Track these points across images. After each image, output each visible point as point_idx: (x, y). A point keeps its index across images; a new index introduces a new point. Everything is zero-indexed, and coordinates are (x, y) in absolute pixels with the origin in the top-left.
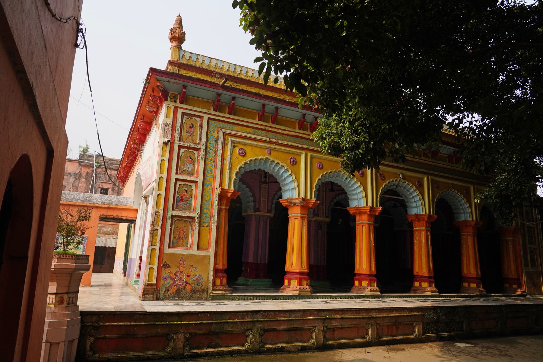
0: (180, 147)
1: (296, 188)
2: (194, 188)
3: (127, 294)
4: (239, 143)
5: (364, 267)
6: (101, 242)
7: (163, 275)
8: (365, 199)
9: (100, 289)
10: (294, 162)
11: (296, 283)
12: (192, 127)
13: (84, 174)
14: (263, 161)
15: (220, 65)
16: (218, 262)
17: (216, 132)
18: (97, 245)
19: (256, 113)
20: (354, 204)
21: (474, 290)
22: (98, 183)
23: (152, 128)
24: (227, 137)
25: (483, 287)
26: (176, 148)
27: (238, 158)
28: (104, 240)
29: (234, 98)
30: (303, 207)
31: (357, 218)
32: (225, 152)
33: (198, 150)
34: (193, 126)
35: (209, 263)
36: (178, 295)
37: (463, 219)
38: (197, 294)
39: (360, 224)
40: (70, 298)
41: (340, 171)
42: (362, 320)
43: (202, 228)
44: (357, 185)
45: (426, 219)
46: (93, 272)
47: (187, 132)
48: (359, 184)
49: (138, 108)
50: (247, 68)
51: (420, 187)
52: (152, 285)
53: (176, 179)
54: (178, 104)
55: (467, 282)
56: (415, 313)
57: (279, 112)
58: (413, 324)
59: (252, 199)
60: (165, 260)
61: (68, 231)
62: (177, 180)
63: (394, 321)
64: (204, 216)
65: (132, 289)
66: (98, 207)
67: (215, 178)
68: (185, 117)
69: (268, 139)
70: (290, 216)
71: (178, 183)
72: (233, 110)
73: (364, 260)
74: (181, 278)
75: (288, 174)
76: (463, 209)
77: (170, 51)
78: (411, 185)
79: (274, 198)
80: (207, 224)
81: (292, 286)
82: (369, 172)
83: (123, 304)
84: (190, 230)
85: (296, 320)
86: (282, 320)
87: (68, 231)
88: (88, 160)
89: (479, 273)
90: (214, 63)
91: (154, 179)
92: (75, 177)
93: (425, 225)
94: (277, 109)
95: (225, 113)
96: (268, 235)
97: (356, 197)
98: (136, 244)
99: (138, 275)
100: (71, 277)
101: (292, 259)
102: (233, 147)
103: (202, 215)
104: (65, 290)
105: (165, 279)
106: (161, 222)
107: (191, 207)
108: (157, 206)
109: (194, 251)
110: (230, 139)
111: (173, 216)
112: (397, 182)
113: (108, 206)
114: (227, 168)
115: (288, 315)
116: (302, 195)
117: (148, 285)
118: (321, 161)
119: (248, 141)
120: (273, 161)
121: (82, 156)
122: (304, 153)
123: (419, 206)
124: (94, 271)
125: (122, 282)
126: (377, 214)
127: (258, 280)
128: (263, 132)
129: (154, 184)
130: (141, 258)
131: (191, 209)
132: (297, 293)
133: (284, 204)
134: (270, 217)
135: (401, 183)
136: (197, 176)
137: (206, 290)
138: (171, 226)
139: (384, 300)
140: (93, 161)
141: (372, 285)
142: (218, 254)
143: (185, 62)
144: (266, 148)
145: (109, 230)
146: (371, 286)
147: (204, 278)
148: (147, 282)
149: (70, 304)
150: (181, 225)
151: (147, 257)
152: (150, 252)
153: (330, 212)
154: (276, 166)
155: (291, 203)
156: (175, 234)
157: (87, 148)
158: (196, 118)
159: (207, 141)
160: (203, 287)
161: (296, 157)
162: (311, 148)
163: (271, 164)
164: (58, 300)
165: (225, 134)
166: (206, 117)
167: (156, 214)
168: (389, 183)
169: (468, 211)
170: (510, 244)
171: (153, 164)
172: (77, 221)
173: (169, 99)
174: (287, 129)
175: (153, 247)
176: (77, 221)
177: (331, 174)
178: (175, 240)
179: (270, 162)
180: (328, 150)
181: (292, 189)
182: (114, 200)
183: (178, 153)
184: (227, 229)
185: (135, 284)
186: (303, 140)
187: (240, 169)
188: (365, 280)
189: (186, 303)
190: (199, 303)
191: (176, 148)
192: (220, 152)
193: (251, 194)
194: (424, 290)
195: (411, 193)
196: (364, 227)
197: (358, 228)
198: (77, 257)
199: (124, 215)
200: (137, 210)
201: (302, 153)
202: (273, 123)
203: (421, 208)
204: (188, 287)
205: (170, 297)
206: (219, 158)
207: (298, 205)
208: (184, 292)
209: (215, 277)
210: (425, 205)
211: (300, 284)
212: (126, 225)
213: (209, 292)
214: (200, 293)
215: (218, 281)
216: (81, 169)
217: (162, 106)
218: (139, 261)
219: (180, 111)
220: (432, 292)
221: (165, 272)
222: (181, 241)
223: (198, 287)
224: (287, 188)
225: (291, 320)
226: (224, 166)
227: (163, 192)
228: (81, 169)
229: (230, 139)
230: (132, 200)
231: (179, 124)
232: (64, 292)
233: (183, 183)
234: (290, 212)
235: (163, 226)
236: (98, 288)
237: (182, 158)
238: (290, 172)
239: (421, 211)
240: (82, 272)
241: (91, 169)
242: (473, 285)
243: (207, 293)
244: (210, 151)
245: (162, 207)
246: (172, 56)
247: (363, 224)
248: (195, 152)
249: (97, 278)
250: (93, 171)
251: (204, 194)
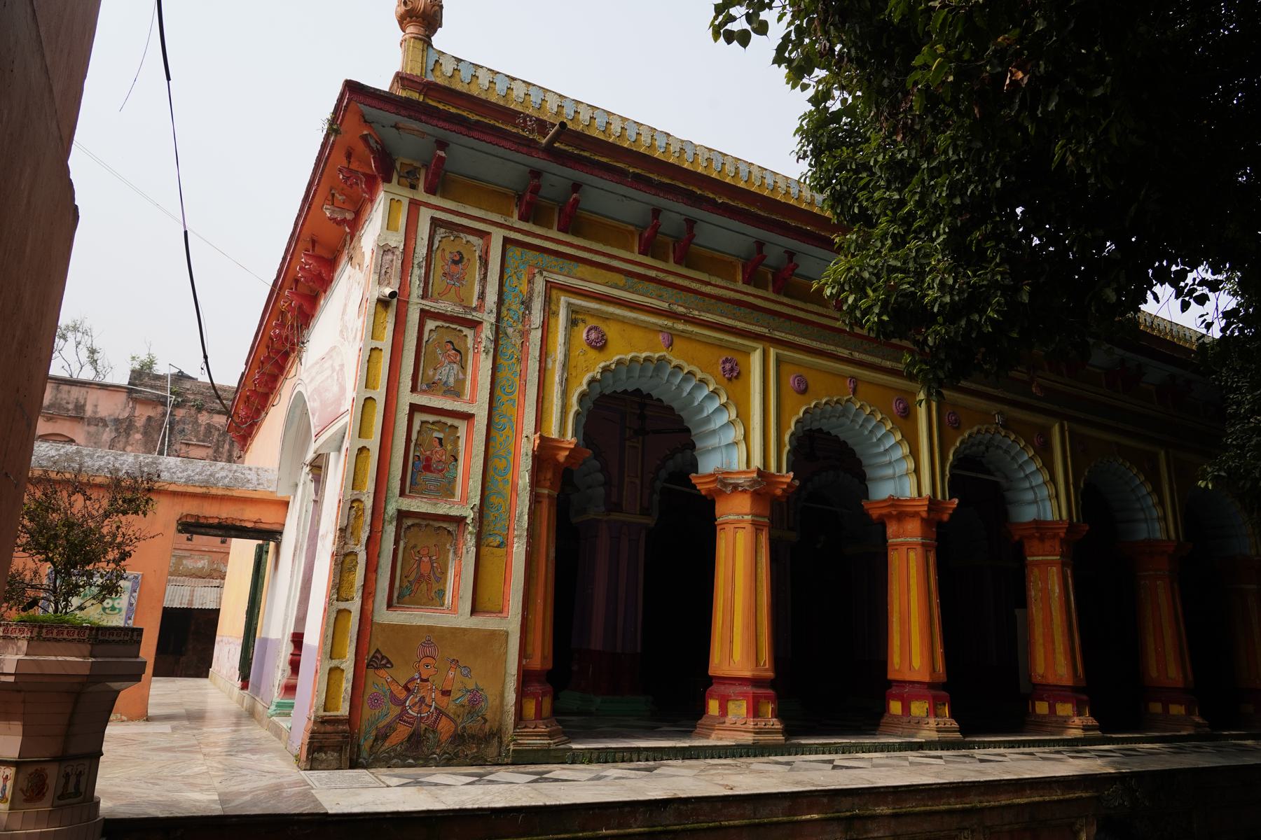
0: (425, 314)
1: (738, 444)
2: (462, 432)
3: (255, 748)
4: (588, 312)
6: (180, 596)
7: (371, 690)
8: (913, 479)
9: (174, 729)
10: (734, 374)
11: (744, 711)
12: (458, 260)
13: (140, 423)
14: (652, 367)
17: (525, 280)
18: (167, 604)
19: (632, 233)
20: (883, 491)
22: (177, 447)
23: (336, 275)
24: (554, 292)
25: (1201, 715)
26: (414, 316)
27: (585, 353)
29: (576, 187)
30: (757, 496)
31: (891, 529)
32: (550, 336)
33: (475, 325)
34: (462, 258)
36: (416, 750)
37: (1143, 535)
38: (473, 747)
40: (67, 776)
41: (848, 401)
43: (484, 550)
44: (892, 441)
45: (1062, 535)
46: (154, 675)
47: (445, 274)
48: (899, 437)
50: (609, 113)
51: (1044, 451)
53: (411, 405)
57: (695, 231)
60: (377, 643)
61: (72, 545)
62: (414, 408)
64: (491, 514)
65: (269, 729)
67: (521, 407)
68: (441, 232)
69: (665, 306)
70: (719, 520)
71: (419, 418)
72: (572, 222)
74: (422, 700)
75: (716, 404)
76: (1142, 509)
78: (1022, 444)
80: (498, 540)
81: (730, 718)
83: (246, 787)
84: (451, 555)
85: (772, 824)
87: (72, 545)
88: (152, 387)
90: (519, 91)
91: (347, 405)
92: (117, 430)
94: (691, 223)
95: (550, 228)
96: (641, 576)
97: (889, 472)
98: (291, 594)
99: (290, 689)
101: (731, 642)
102: (573, 323)
106: (367, 529)
108: (356, 481)
109: (462, 619)
111: (402, 515)
112: (988, 436)
113: (204, 490)
114: (557, 379)
116: (757, 462)
119: (611, 309)
120: (679, 367)
123: (1043, 500)
124: (156, 673)
125: (234, 706)
126: (946, 517)
128: (652, 286)
129: (346, 419)
130: (298, 639)
131: (453, 495)
132: (748, 739)
133: (703, 488)
135: (999, 437)
137: (497, 734)
138: (396, 542)
139: (978, 753)
141: (939, 712)
143: (439, 81)
144: (661, 330)
145: (200, 565)
146: (936, 716)
147: (490, 699)
148: (321, 713)
151: (324, 636)
152: (332, 620)
155: (726, 485)
157: (152, 362)
158: (471, 238)
159: (500, 302)
161: (739, 358)
163: (673, 374)
165: (550, 286)
166: (497, 236)
167: (352, 506)
168: (970, 436)
169: (1155, 514)
171: (342, 366)
172: (107, 515)
174: (714, 280)
175: (342, 605)
176: (107, 515)
177: (828, 408)
179: (669, 369)
182: (223, 474)
183: (420, 330)
184: (552, 554)
185: (279, 715)
188: (919, 698)
189: (440, 776)
190: (481, 776)
191: (414, 316)
192: (536, 336)
194: (1063, 724)
196: (912, 554)
197: (895, 558)
198: (99, 637)
199: (249, 516)
200: (287, 504)
201: (755, 349)
202: (678, 262)
203: (1048, 504)
204: (445, 726)
205: (391, 758)
206: (535, 352)
207: (744, 491)
209: (521, 694)
210: (1057, 496)
211: (755, 712)
213: (506, 739)
215: (530, 708)
216: (134, 408)
217: (372, 201)
219: (425, 215)
221: (379, 681)
222: (424, 586)
223: (473, 726)
224: (713, 442)
225: (759, 825)
226: (548, 374)
227: (374, 443)
228: (134, 408)
230: (274, 476)
231: (422, 251)
233: (431, 418)
234: (720, 508)
235: (373, 543)
236: (166, 727)
238: (724, 400)
240: (115, 685)
241: (160, 409)
242: (1177, 710)
243: (501, 742)
244: (510, 331)
245: (370, 486)
246: (405, 63)
247: (910, 547)
248: (466, 331)
249: (165, 692)
250: (164, 415)
251: (491, 451)
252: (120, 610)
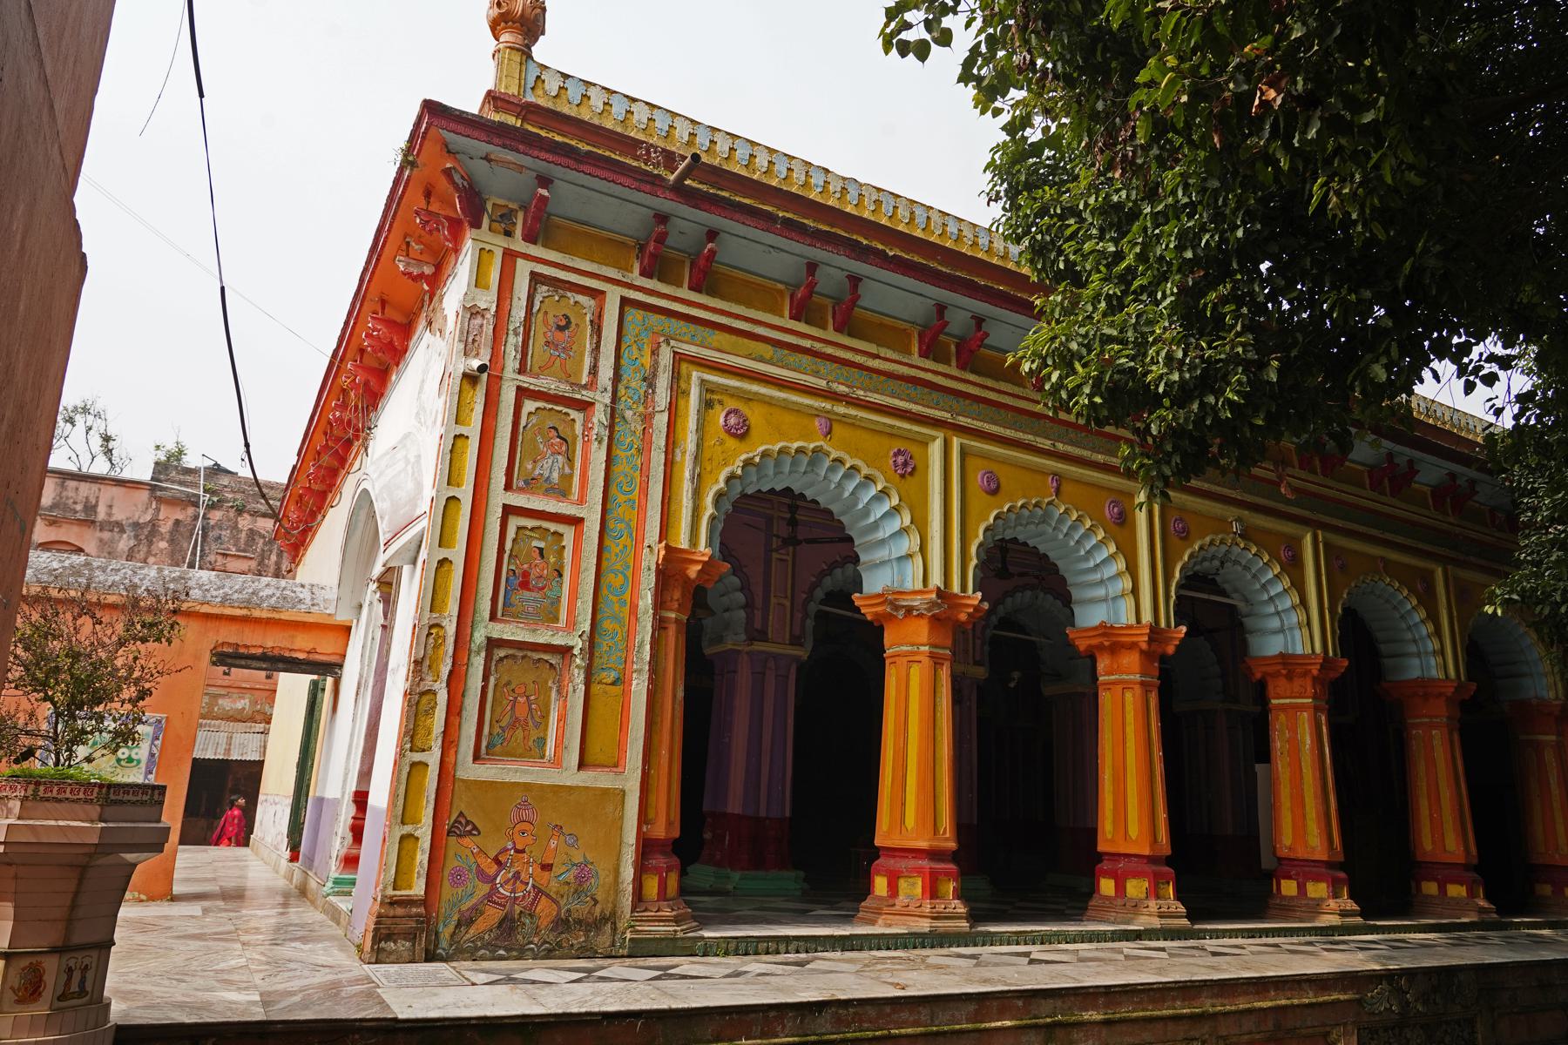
4: (725, 390)
5: (1133, 831)
6: (210, 746)
7: (452, 863)
8: (1130, 601)
9: (206, 911)
10: (908, 469)
11: (919, 890)
13: (165, 528)
14: (805, 460)
15: (662, 123)
16: (651, 814)
17: (647, 351)
18: (198, 754)
19: (781, 292)
20: (1090, 616)
21: (1459, 906)
22: (212, 558)
23: (411, 344)
24: (684, 366)
25: (1488, 897)
26: (508, 396)
27: (722, 442)
28: (222, 737)
29: (712, 235)
30: (936, 621)
31: (1102, 665)
32: (679, 421)
33: (585, 406)
35: (622, 818)
36: (508, 939)
37: (1415, 673)
38: (579, 935)
39: (1114, 683)
40: (70, 971)
41: (1050, 503)
42: (1171, 1026)
43: (595, 688)
44: (1104, 554)
45: (1315, 672)
46: (182, 842)
47: (547, 343)
48: (1113, 549)
49: (365, 270)
51: (1293, 566)
52: (408, 902)
53: (505, 507)
54: (519, 245)
55: (1435, 879)
56: (1334, 997)
58: (1327, 1034)
59: (740, 597)
62: (508, 510)
63: (1270, 1025)
64: (603, 644)
65: (324, 911)
66: (208, 617)
67: (642, 509)
68: (543, 290)
69: (822, 384)
71: (514, 522)
73: (1128, 803)
74: (517, 876)
75: (886, 507)
76: (1415, 641)
77: (491, 66)
78: (1266, 558)
79: (810, 598)
80: (613, 675)
81: (902, 899)
82: (1521, 382)
83: (295, 984)
84: (554, 694)
85: (954, 1032)
86: (907, 1036)
88: (181, 483)
89: (1474, 850)
92: (136, 537)
93: (1310, 690)
94: (855, 280)
95: (679, 285)
98: (342, 745)
99: (351, 861)
100: (80, 881)
101: (903, 804)
102: (707, 405)
103: (597, 639)
104: (53, 937)
105: (458, 878)
106: (449, 662)
107: (558, 611)
108: (435, 601)
109: (569, 776)
110: (694, 374)
112: (1224, 548)
113: (244, 612)
114: (687, 474)
115: (924, 1013)
116: (936, 580)
117: (393, 903)
118: (994, 467)
119: (755, 388)
121: (161, 468)
122: (940, 435)
123: (1291, 629)
125: (281, 883)
127: (761, 873)
128: (806, 360)
130: (361, 799)
131: (556, 619)
132: (924, 926)
133: (868, 612)
134: (796, 659)
135: (1236, 550)
136: (582, 501)
137: (611, 918)
138: (486, 678)
140: (196, 485)
141: (1161, 892)
142: (653, 782)
145: (239, 705)
146: (1158, 897)
148: (390, 892)
149: (73, 996)
150: (520, 675)
151: (394, 795)
153: (987, 648)
154: (847, 476)
155: (897, 608)
156: (499, 710)
157: (181, 452)
158: (581, 298)
159: (617, 378)
160: (598, 909)
161: (914, 449)
162: (963, 421)
163: (831, 469)
164: (15, 981)
165: (679, 358)
166: (614, 295)
167: (429, 632)
168: (1201, 548)
170: (1549, 756)
173: (486, 222)
174: (884, 352)
175: (417, 757)
176: (121, 643)
177: (1026, 512)
178: (497, 730)
179: (827, 463)
180: (1091, 396)
181: (900, 559)
184: (680, 694)
185: (337, 894)
186: (935, 395)
187: (728, 480)
188: (1137, 875)
190: (589, 971)
191: (508, 396)
192: (661, 420)
193: (736, 580)
194: (1316, 908)
195: (1264, 586)
196: (1129, 695)
198: (111, 796)
199: (300, 645)
200: (349, 628)
201: (934, 438)
203: (1297, 633)
204: (545, 909)
205: (477, 949)
206: (660, 440)
207: (920, 616)
208: (527, 929)
209: (641, 869)
210: (1309, 624)
211: (933, 892)
212: (304, 680)
213: (621, 925)
214: (587, 931)
215: (652, 886)
216: (158, 510)
217: (457, 251)
218: (352, 810)
219: (523, 269)
220: (1344, 914)
221: (461, 852)
222: (519, 733)
223: (580, 909)
225: (937, 1034)
227: (458, 554)
229: (696, 375)
231: (519, 314)
232: (42, 944)
235: (456, 679)
236: (195, 909)
237: (529, 435)
239: (1299, 645)
240: (130, 857)
241: (191, 511)
242: (1456, 891)
243: (614, 929)
244: (629, 414)
245: (453, 607)
246: (499, 79)
247: (1127, 687)
248: (574, 414)
249: (194, 864)
250: (196, 518)
251: (605, 564)
252: (139, 762)
